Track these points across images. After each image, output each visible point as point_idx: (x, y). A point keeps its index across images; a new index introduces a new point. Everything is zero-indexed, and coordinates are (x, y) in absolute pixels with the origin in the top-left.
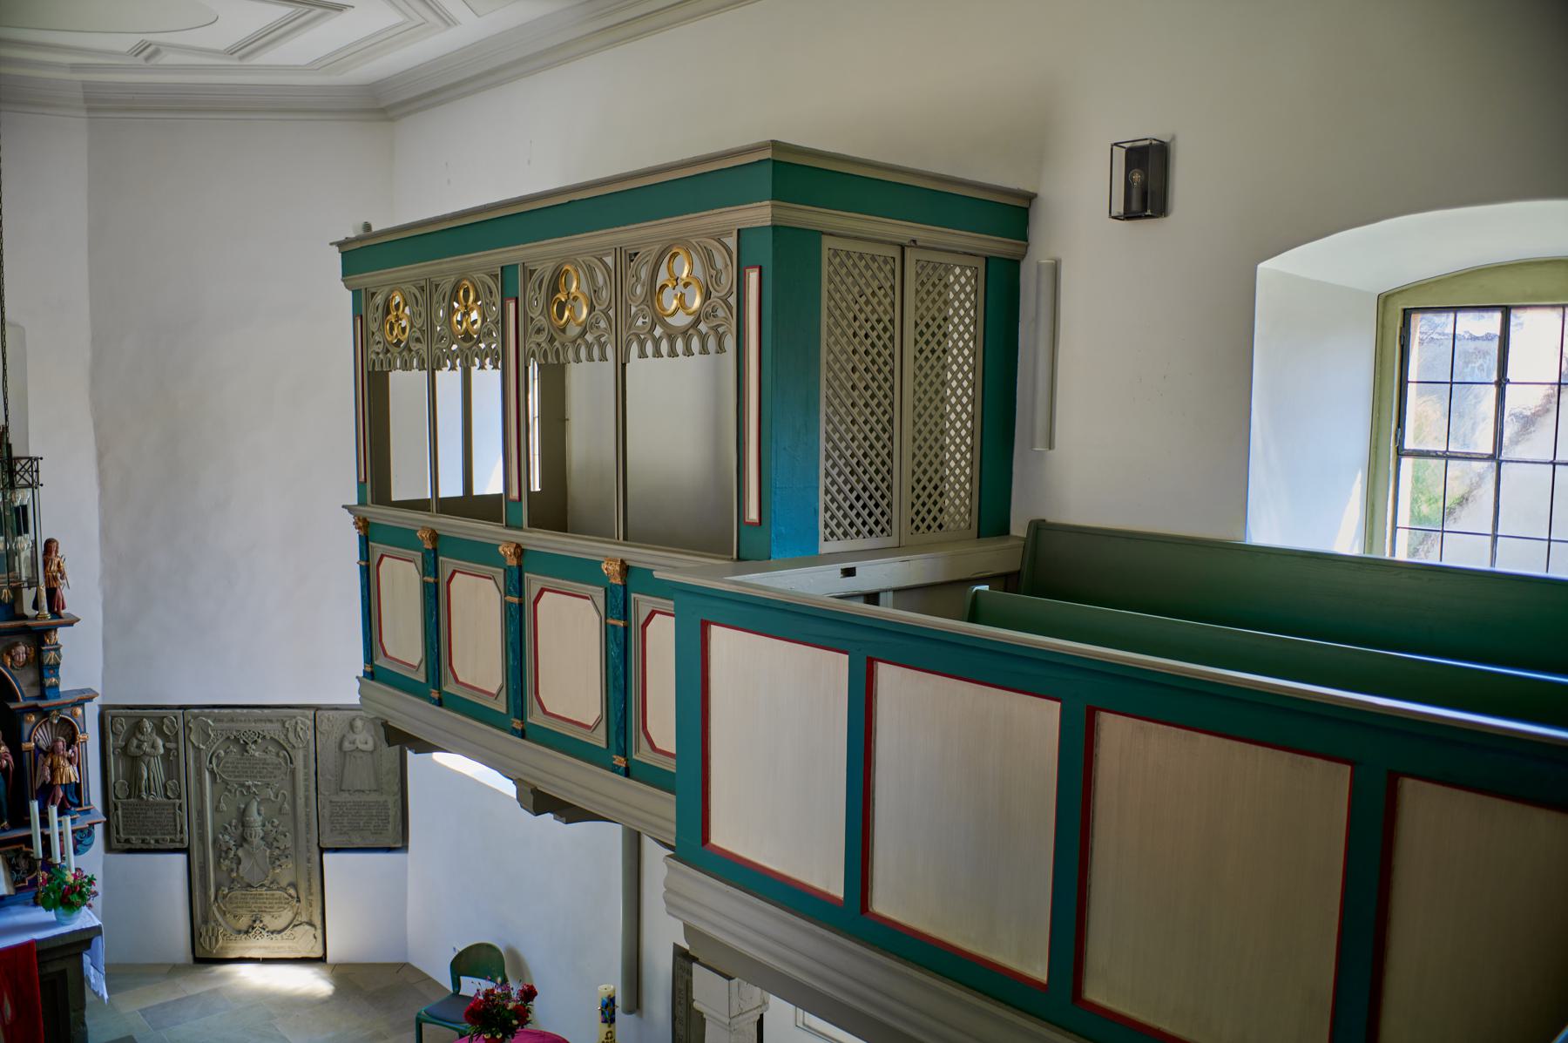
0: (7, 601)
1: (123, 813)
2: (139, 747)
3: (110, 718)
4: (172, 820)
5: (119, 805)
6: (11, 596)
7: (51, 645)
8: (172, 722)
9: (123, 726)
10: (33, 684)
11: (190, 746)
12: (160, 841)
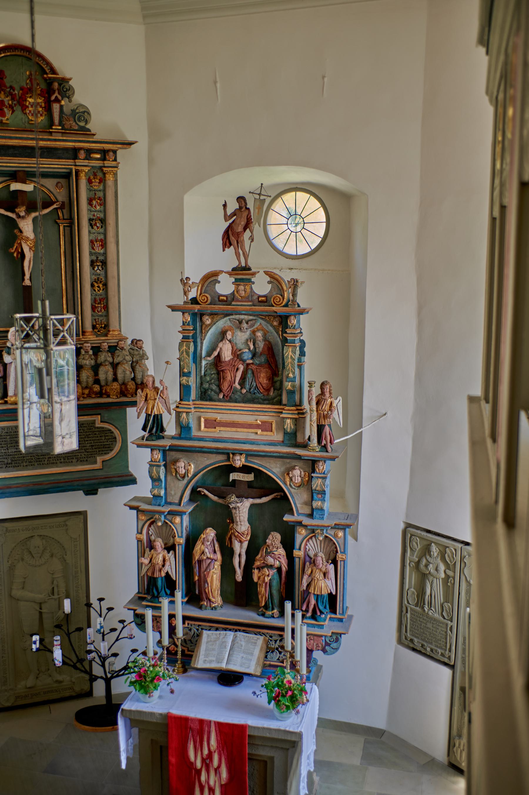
0: (289, 431)
1: (411, 617)
2: (426, 566)
3: (409, 535)
4: (443, 637)
5: (409, 609)
6: (293, 427)
7: (320, 474)
8: (453, 554)
9: (418, 546)
10: (306, 503)
11: (463, 578)
12: (434, 651)
